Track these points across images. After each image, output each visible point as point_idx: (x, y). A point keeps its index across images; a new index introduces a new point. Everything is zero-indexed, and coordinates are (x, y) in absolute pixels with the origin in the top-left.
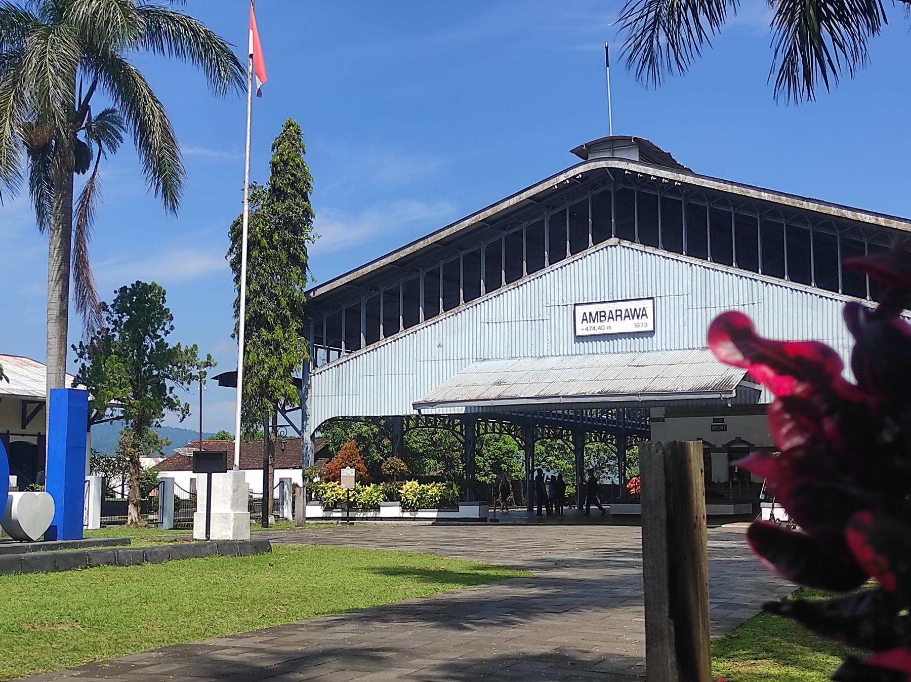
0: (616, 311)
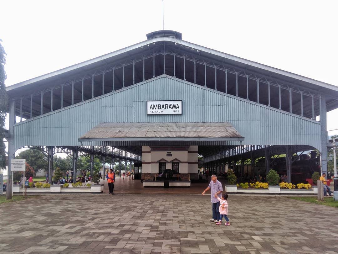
0: (166, 105)
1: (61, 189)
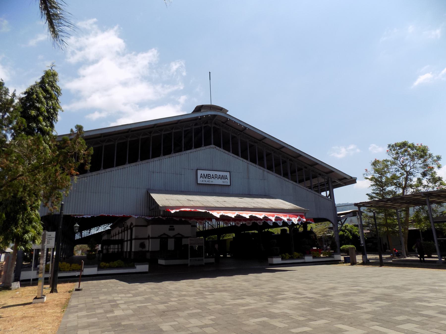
0: (215, 175)
1: (98, 270)
